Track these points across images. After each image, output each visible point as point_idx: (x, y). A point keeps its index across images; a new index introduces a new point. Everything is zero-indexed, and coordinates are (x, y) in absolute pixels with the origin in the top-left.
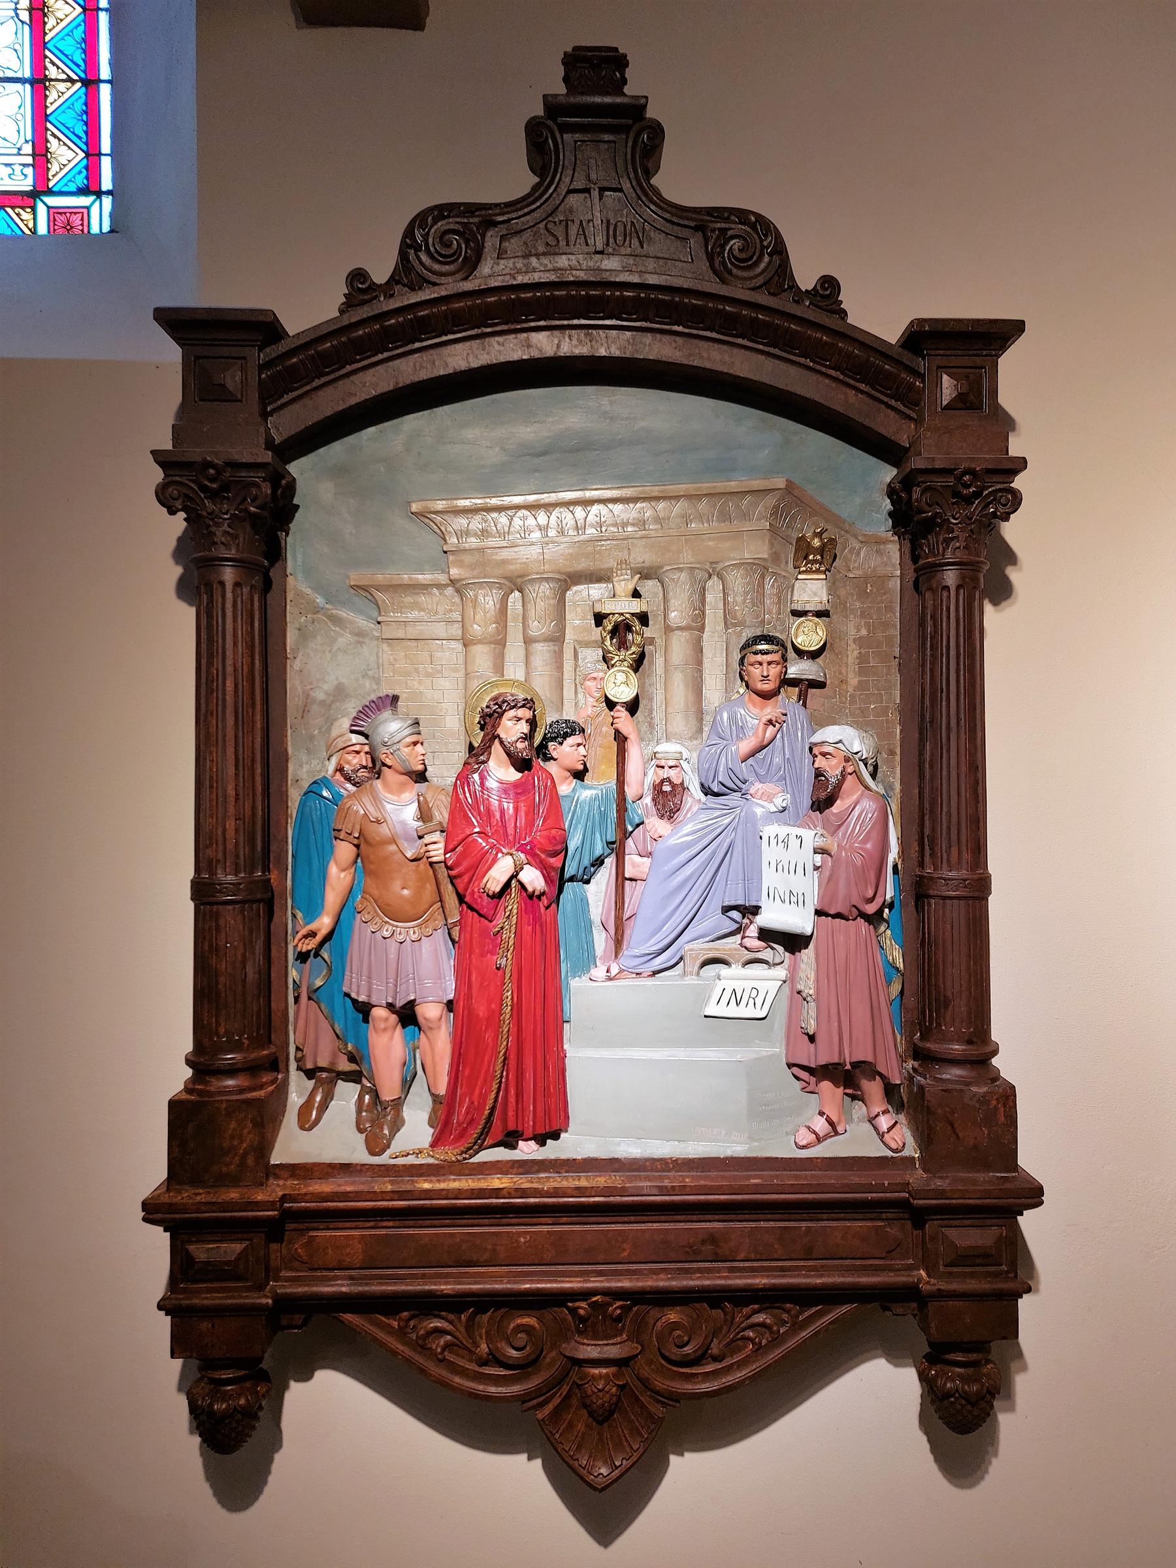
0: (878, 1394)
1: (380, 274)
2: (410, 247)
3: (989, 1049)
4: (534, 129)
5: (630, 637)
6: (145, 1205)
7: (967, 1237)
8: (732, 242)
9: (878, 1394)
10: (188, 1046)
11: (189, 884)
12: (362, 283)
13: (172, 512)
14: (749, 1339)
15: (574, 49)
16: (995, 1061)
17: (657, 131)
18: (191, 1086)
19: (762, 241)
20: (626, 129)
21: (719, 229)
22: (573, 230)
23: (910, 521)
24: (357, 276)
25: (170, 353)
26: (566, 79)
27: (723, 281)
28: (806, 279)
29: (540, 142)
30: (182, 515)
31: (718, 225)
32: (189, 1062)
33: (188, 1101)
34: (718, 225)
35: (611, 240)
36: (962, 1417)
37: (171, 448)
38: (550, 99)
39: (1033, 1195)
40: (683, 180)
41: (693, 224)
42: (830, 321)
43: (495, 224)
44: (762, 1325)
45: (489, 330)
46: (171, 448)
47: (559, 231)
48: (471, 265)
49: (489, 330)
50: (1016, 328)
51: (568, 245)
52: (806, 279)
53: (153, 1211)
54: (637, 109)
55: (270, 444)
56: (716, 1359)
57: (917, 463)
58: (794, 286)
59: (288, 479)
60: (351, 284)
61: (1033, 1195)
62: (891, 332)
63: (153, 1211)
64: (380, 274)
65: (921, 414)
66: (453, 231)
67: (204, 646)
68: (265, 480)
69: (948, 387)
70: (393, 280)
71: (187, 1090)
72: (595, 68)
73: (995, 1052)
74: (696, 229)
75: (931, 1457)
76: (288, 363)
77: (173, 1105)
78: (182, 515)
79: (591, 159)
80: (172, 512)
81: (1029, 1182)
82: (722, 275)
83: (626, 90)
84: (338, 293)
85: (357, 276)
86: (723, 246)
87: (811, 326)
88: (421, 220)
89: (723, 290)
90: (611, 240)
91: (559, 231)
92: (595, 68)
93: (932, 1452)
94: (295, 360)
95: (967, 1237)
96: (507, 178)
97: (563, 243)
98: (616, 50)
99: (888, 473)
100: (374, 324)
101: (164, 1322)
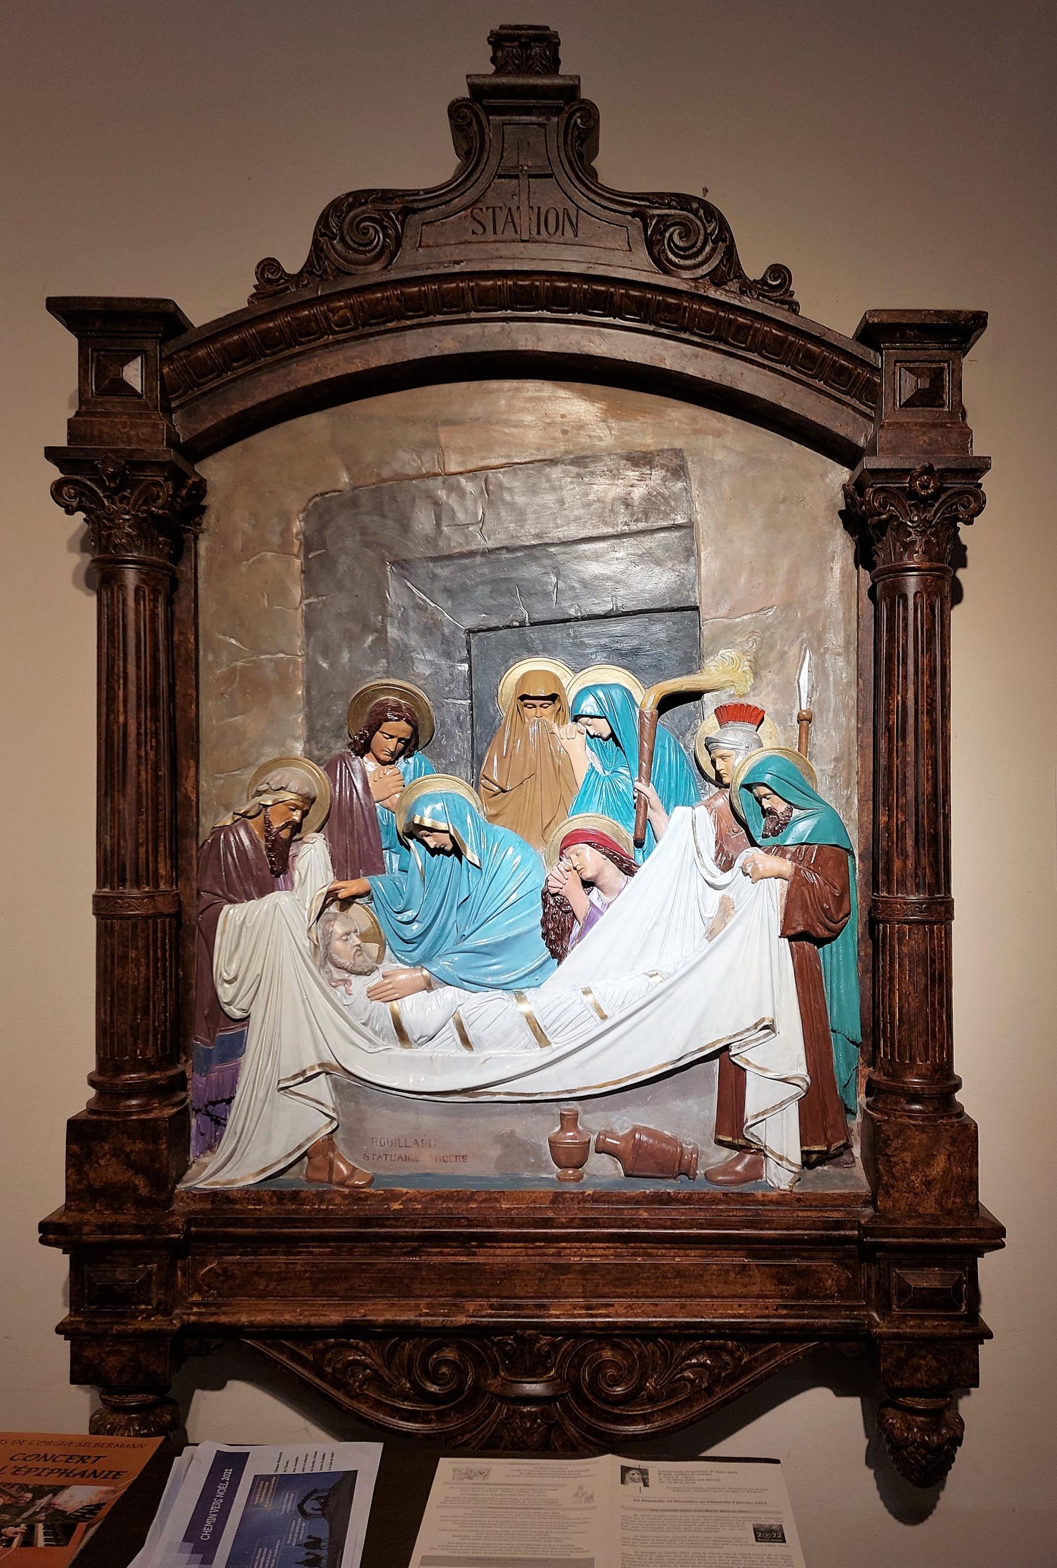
0: (818, 1428)
1: (293, 263)
2: (323, 235)
3: (953, 1083)
4: (455, 110)
5: (395, 594)
6: (43, 1227)
7: (926, 1279)
8: (671, 230)
9: (818, 1428)
10: (89, 1063)
11: (91, 899)
12: (272, 273)
13: (70, 511)
14: (688, 1379)
15: (502, 27)
16: (959, 1096)
17: (590, 112)
18: (97, 1078)
19: (705, 229)
20: (558, 111)
21: (658, 215)
22: (501, 216)
23: (864, 525)
24: (268, 266)
25: (66, 345)
26: (493, 60)
27: (666, 272)
28: (754, 270)
29: (471, 118)
30: (80, 515)
31: (658, 212)
32: (92, 1083)
33: (89, 1121)
34: (658, 212)
35: (543, 228)
36: (913, 1466)
37: (65, 444)
38: (477, 81)
39: (993, 1236)
40: (619, 165)
41: (630, 210)
42: (780, 314)
43: (415, 211)
44: (703, 1365)
45: (408, 322)
46: (65, 444)
47: (487, 217)
48: (390, 252)
49: (408, 322)
50: (979, 320)
51: (495, 233)
52: (754, 270)
53: (51, 1232)
54: (571, 91)
55: (173, 442)
56: (652, 1399)
57: (869, 463)
58: (740, 276)
59: (194, 479)
60: (262, 274)
61: (993, 1236)
62: (844, 325)
63: (51, 1232)
64: (293, 263)
65: (878, 409)
66: (361, 220)
67: (104, 645)
68: (166, 479)
69: (908, 384)
70: (308, 268)
71: (90, 1111)
72: (525, 48)
73: (958, 1086)
74: (634, 215)
75: (877, 1494)
76: (227, 341)
77: (72, 1124)
78: (80, 515)
79: (535, 138)
80: (70, 511)
81: (992, 1222)
82: (663, 266)
83: (562, 71)
84: (249, 284)
85: (268, 266)
86: (662, 234)
87: (757, 321)
88: (336, 208)
89: (661, 280)
90: (543, 228)
91: (487, 217)
92: (525, 48)
93: (878, 1489)
94: (271, 325)
95: (926, 1279)
96: (428, 160)
97: (490, 228)
98: (547, 28)
99: (842, 475)
100: (284, 314)
101: (63, 1347)
